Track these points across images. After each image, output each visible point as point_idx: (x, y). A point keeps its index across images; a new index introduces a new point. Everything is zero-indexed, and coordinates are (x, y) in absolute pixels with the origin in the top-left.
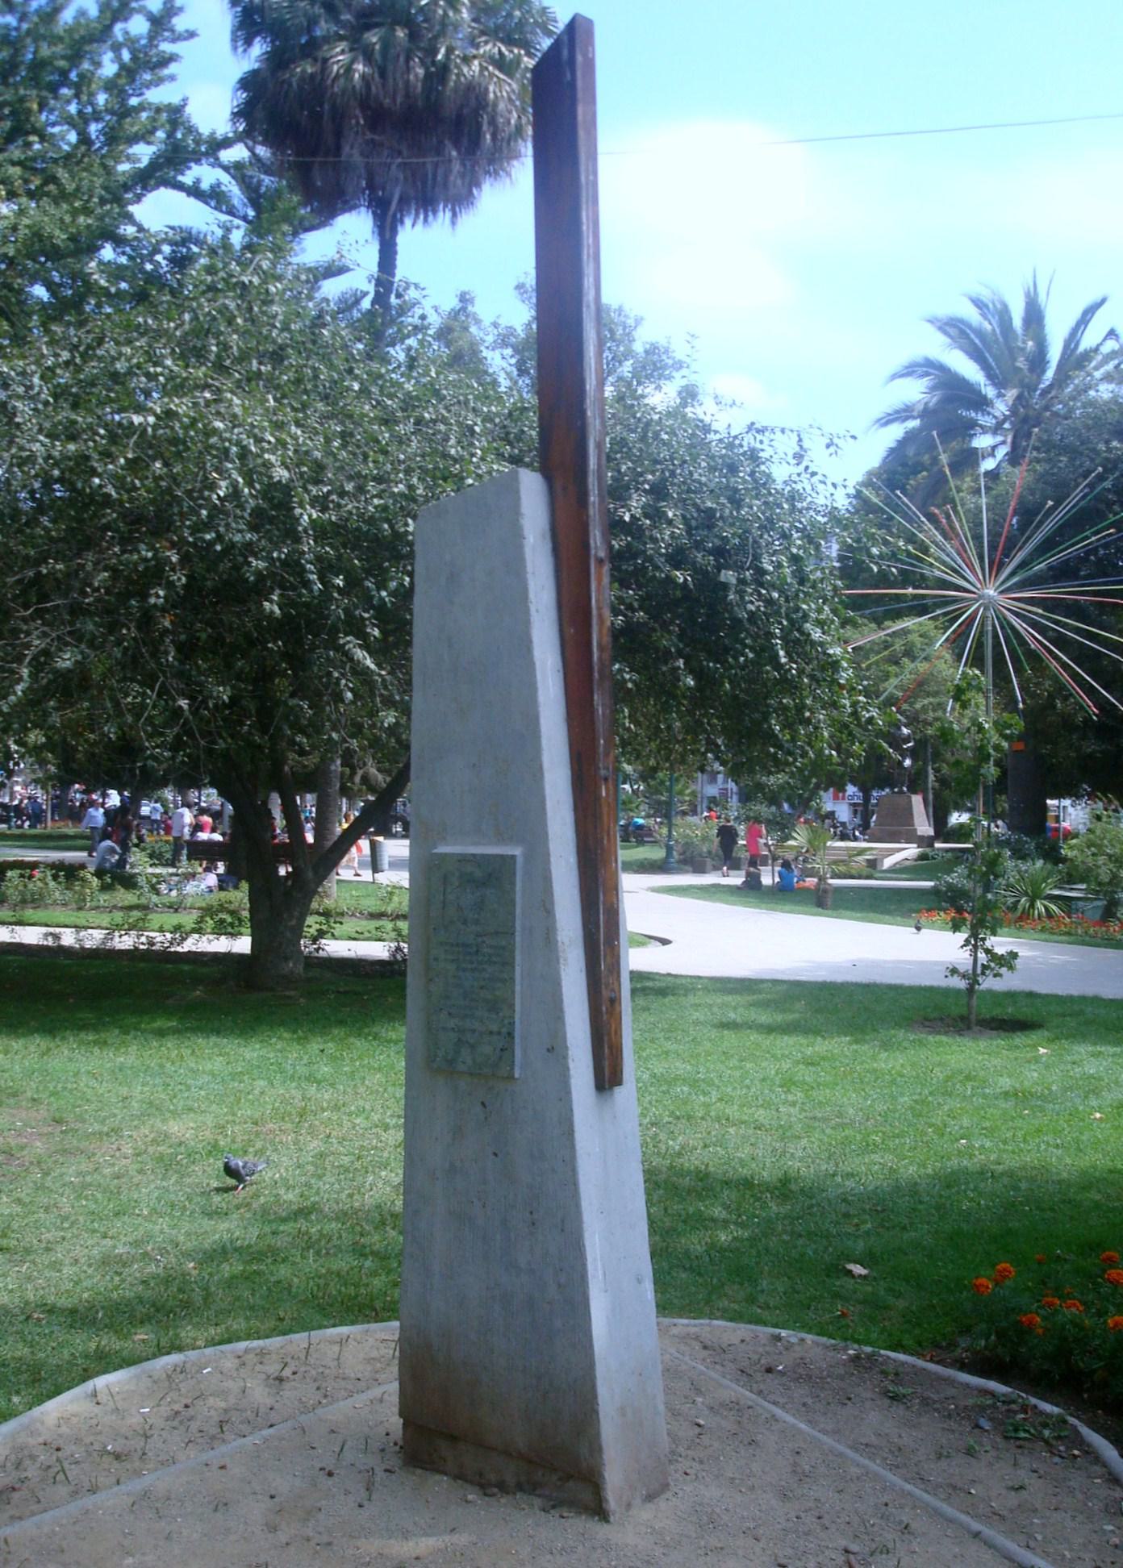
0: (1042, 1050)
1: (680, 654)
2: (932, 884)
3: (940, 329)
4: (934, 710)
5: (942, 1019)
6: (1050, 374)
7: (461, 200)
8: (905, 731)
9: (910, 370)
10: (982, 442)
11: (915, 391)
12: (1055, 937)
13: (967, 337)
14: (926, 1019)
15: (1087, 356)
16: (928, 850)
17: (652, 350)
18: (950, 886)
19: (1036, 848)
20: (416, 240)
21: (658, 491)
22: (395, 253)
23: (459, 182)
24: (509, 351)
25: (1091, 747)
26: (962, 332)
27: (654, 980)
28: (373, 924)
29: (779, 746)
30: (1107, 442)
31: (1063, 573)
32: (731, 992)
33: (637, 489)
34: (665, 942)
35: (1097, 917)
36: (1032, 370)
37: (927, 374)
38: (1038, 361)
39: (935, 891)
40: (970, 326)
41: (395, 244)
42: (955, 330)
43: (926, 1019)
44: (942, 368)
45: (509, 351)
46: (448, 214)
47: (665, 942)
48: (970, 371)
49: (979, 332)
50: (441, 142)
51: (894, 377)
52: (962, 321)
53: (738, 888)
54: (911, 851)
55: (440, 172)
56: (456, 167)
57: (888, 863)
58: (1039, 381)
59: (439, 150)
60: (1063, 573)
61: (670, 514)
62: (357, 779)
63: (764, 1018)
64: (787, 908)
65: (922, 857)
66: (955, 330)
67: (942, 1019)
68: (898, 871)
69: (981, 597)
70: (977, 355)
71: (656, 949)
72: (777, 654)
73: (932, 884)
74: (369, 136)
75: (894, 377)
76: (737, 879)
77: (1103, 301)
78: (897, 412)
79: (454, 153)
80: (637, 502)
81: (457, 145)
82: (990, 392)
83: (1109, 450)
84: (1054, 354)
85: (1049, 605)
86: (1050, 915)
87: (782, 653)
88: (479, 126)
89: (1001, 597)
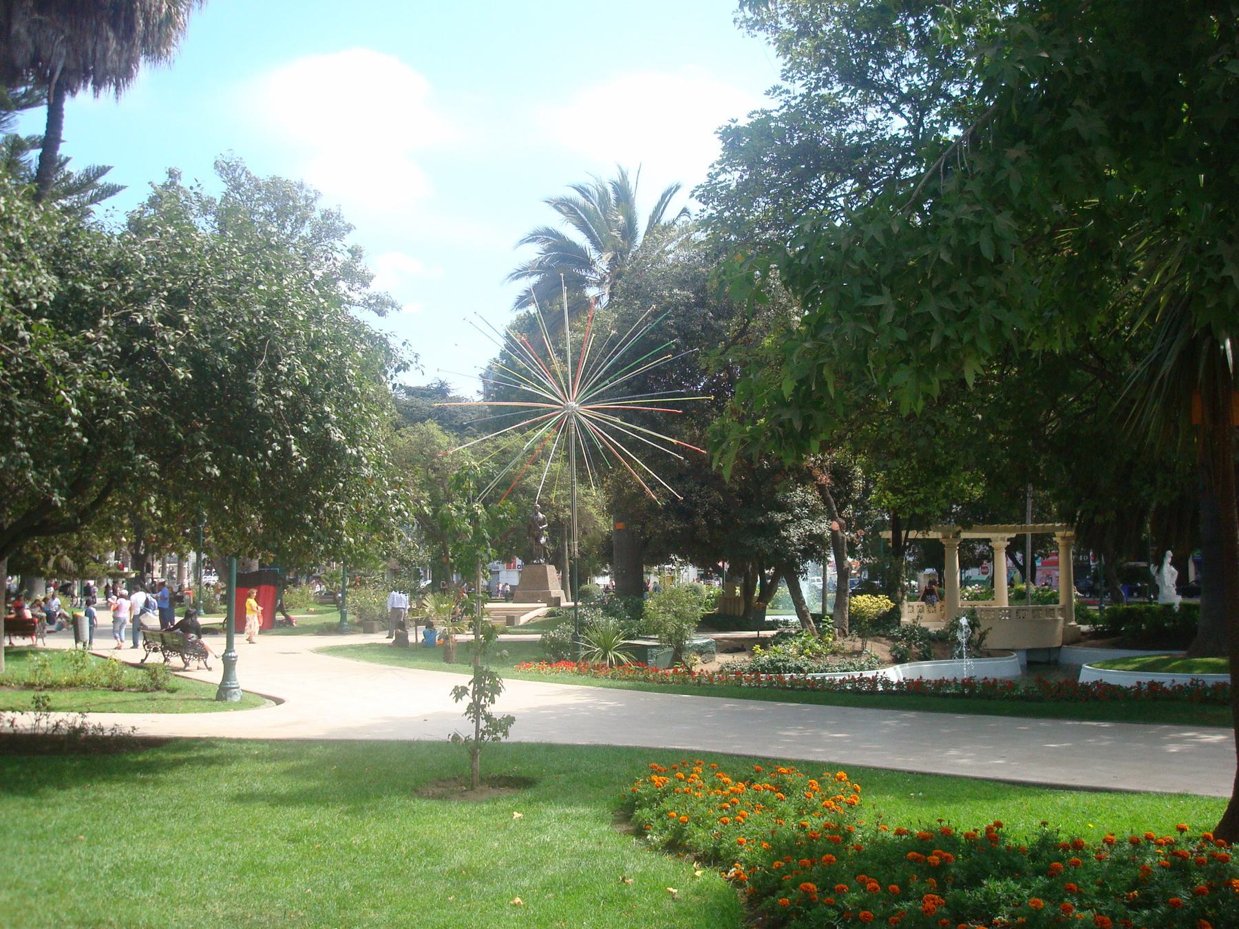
0: (517, 815)
1: (208, 447)
2: (539, 636)
3: (555, 207)
4: (565, 499)
5: (455, 779)
6: (639, 241)
7: (121, 75)
8: (541, 515)
9: (534, 238)
10: (591, 292)
11: (534, 252)
12: (620, 683)
13: (576, 213)
14: (440, 780)
15: (668, 227)
16: (555, 609)
17: (327, 215)
18: (552, 639)
19: (626, 606)
20: (82, 106)
21: (178, 299)
22: (62, 116)
23: (115, 57)
24: (211, 218)
25: (673, 525)
26: (571, 209)
27: (214, 746)
28: (28, 696)
29: (311, 534)
30: (671, 289)
31: (639, 386)
32: (273, 758)
33: (157, 295)
34: (279, 701)
35: (669, 661)
36: (623, 238)
37: (548, 240)
38: (629, 231)
39: (541, 644)
40: (577, 205)
41: (61, 109)
42: (565, 206)
43: (440, 780)
44: (558, 235)
45: (211, 218)
46: (113, 88)
47: (279, 701)
48: (578, 238)
49: (584, 210)
50: (99, 24)
51: (522, 242)
52: (571, 201)
53: (389, 646)
54: (541, 609)
55: (99, 47)
56: (113, 44)
57: (523, 620)
58: (630, 247)
59: (97, 33)
60: (639, 386)
61: (186, 319)
62: (51, 564)
63: (283, 788)
64: (419, 662)
65: (550, 614)
66: (565, 206)
67: (455, 779)
68: (528, 626)
69: (565, 408)
70: (584, 227)
71: (270, 710)
72: (290, 449)
73: (539, 636)
74: (36, 16)
75: (522, 242)
76: (381, 638)
77: (678, 187)
78: (525, 269)
79: (111, 34)
80: (154, 308)
81: (114, 27)
82: (594, 255)
83: (671, 296)
84: (642, 226)
85: (628, 416)
86: (620, 662)
87: (294, 447)
88: (133, 12)
89: (582, 408)
